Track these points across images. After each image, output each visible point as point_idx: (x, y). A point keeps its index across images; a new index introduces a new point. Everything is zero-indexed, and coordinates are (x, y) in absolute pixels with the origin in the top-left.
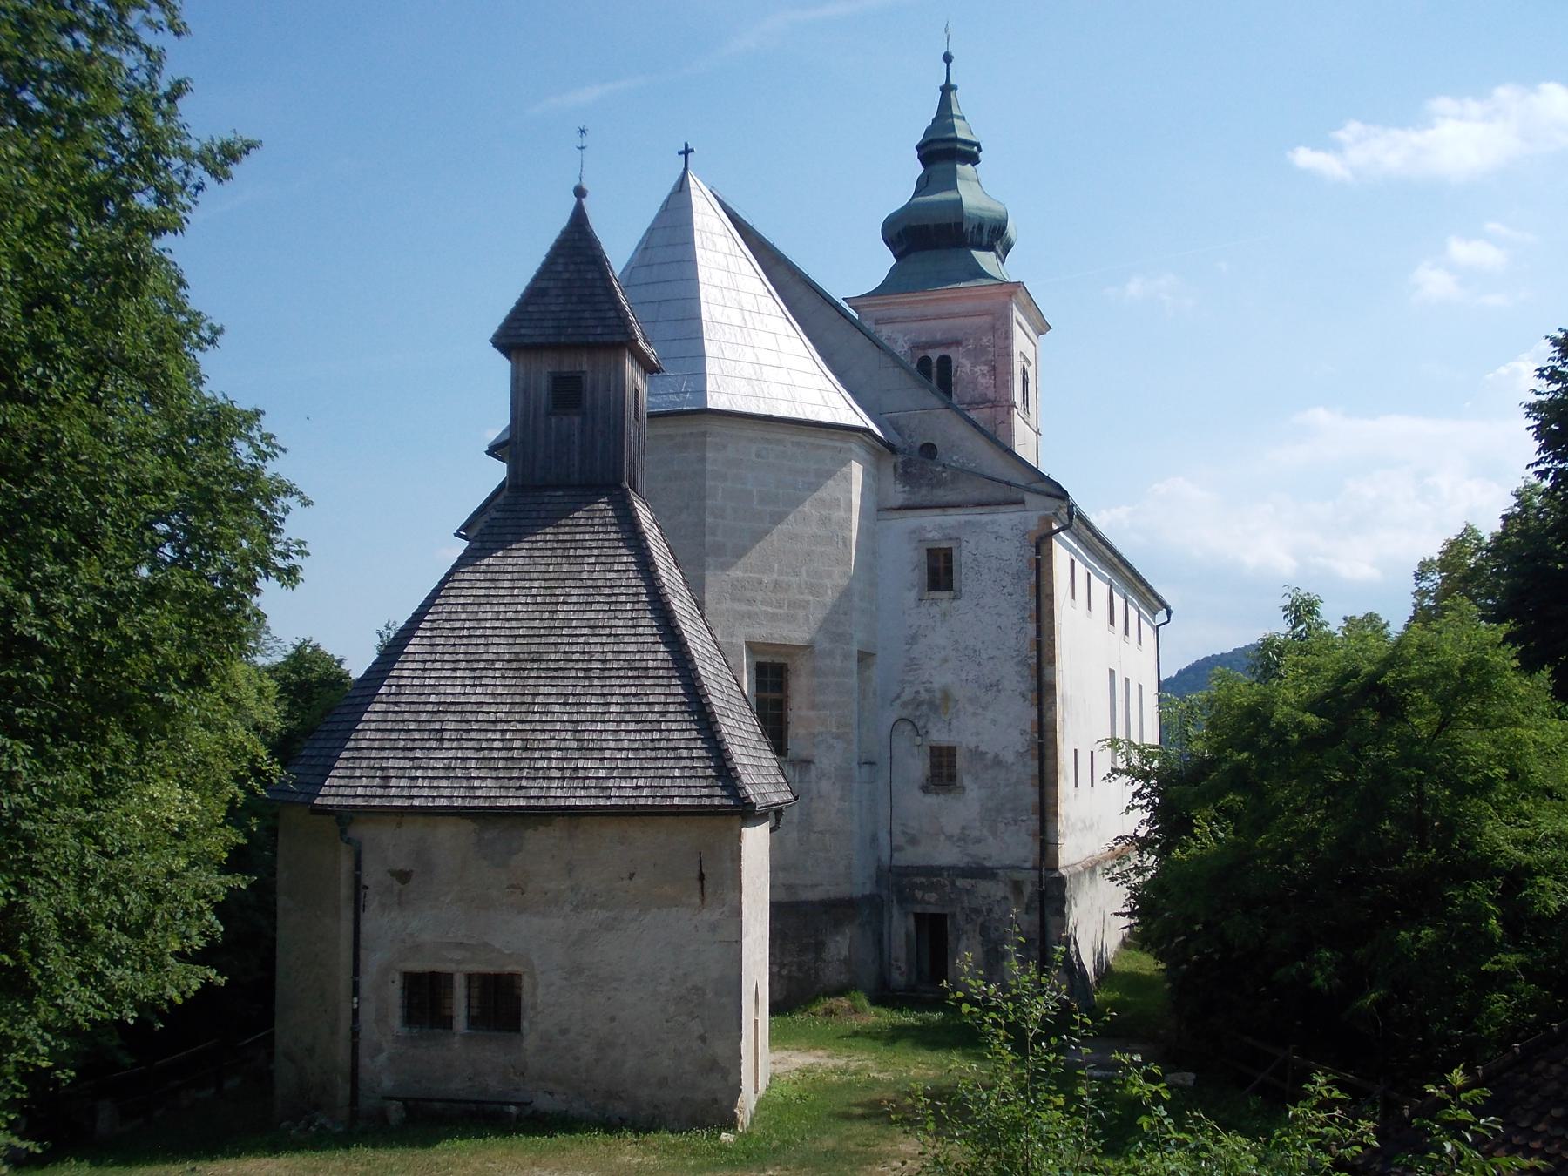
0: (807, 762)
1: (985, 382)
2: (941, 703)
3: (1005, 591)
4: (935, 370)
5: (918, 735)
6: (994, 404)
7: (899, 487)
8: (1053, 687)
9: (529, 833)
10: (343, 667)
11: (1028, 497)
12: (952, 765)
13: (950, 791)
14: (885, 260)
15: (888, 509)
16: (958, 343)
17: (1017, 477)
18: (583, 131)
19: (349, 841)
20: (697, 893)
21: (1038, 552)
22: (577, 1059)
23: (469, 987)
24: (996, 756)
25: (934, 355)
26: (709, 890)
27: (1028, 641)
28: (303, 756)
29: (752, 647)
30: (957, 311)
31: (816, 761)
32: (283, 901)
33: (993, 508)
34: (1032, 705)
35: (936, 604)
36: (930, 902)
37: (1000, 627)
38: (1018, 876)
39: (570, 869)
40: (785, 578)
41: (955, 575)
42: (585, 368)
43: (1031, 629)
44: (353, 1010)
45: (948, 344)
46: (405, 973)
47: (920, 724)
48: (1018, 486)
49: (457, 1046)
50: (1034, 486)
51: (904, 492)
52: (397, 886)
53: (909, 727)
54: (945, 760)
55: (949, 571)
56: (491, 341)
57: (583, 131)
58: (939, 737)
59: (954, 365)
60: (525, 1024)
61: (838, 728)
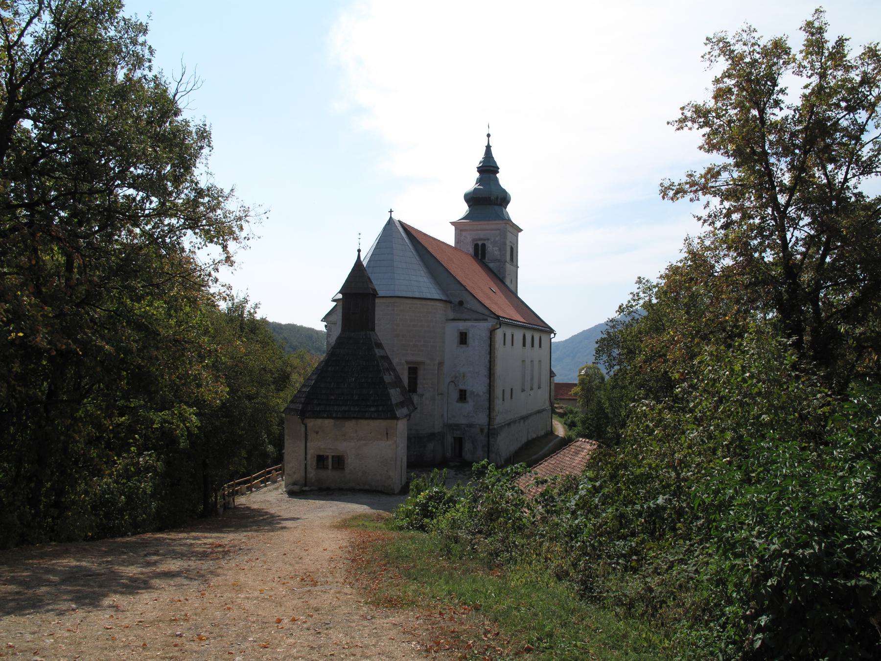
8: (494, 374)
10: (199, 186)
11: (489, 318)
12: (465, 395)
23: (333, 460)
25: (480, 243)
29: (407, 363)
32: (286, 437)
43: (488, 356)
45: (485, 240)
58: (462, 387)
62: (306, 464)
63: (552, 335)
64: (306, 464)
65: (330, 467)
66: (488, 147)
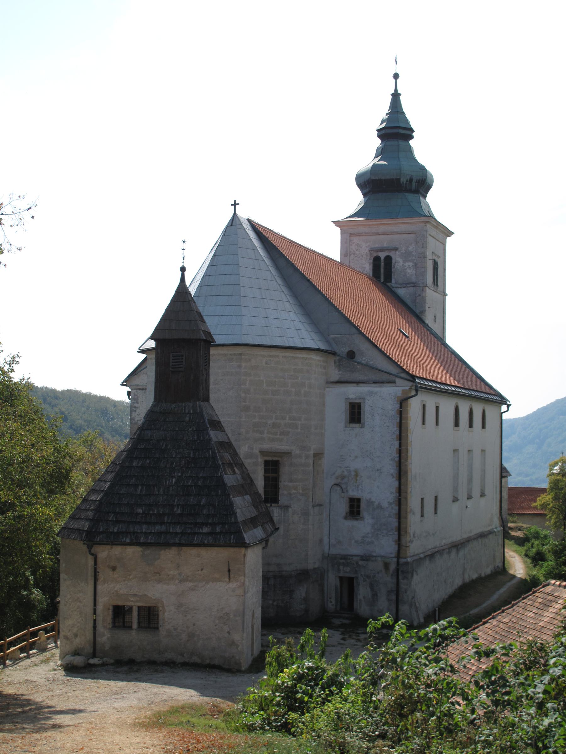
0: (287, 507)
1: (410, 272)
3: (385, 425)
4: (382, 264)
5: (343, 492)
6: (415, 285)
7: (337, 372)
9: (162, 552)
11: (397, 380)
12: (359, 506)
13: (357, 519)
14: (379, 141)
16: (396, 249)
17: (393, 370)
19: (92, 554)
20: (227, 576)
21: (401, 407)
22: (181, 640)
24: (379, 504)
25: (382, 255)
26: (232, 576)
27: (395, 449)
30: (396, 230)
31: (292, 506)
32: (63, 576)
33: (380, 384)
34: (396, 480)
35: (353, 429)
36: (346, 571)
39: (178, 566)
40: (278, 421)
41: (362, 416)
45: (390, 250)
47: (343, 486)
48: (392, 375)
49: (134, 634)
50: (399, 375)
51: (339, 374)
54: (355, 504)
55: (359, 413)
57: (184, 242)
58: (354, 494)
59: (393, 261)
61: (303, 491)
62: (95, 621)
63: (504, 408)
64: (95, 621)
65: (135, 626)
66: (396, 96)
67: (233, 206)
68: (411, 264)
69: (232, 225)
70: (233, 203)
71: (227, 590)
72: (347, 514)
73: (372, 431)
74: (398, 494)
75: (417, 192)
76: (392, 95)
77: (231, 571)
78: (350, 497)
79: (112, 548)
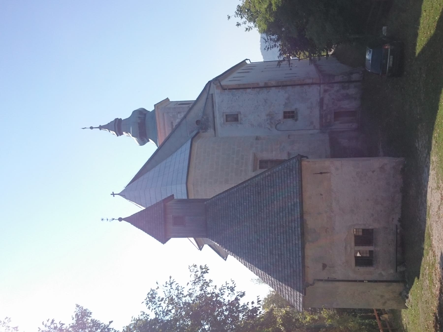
2: (271, 116)
5: (280, 123)
7: (209, 131)
11: (210, 93)
12: (289, 112)
13: (297, 113)
15: (215, 134)
16: (172, 123)
18: (102, 220)
19: (314, 283)
20: (326, 174)
21: (226, 89)
22: (381, 211)
28: (288, 299)
37: (248, 100)
38: (322, 91)
41: (233, 113)
42: (171, 216)
43: (249, 90)
44: (368, 282)
46: (355, 266)
51: (210, 129)
52: (327, 268)
53: (278, 125)
56: (164, 244)
57: (102, 220)
58: (281, 116)
60: (370, 228)
62: (369, 281)
63: (248, 62)
64: (369, 281)
65: (371, 248)
66: (101, 128)
67: (115, 195)
68: (179, 115)
69: (125, 196)
70: (113, 195)
71: (337, 175)
72: (294, 119)
73: (242, 107)
74: (280, 87)
75: (145, 115)
76: (100, 129)
77: (321, 172)
78: (283, 118)
79: (308, 267)
